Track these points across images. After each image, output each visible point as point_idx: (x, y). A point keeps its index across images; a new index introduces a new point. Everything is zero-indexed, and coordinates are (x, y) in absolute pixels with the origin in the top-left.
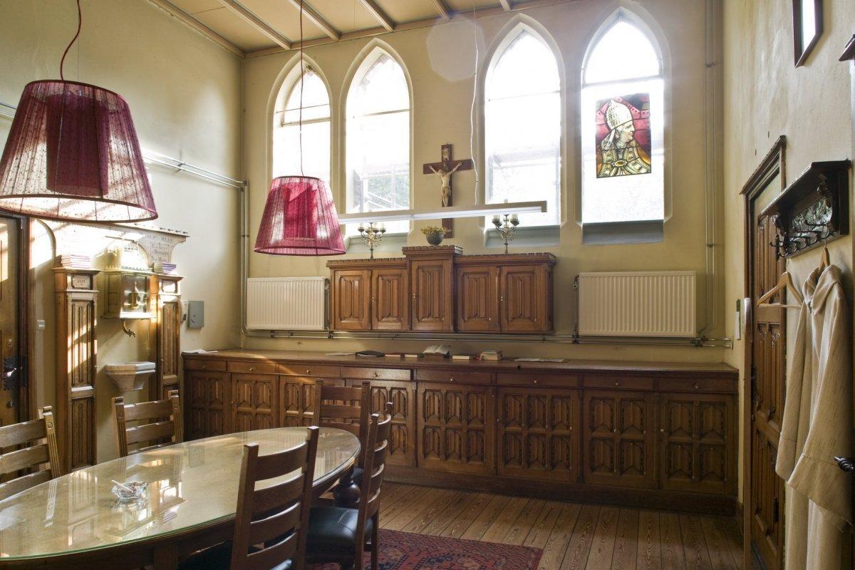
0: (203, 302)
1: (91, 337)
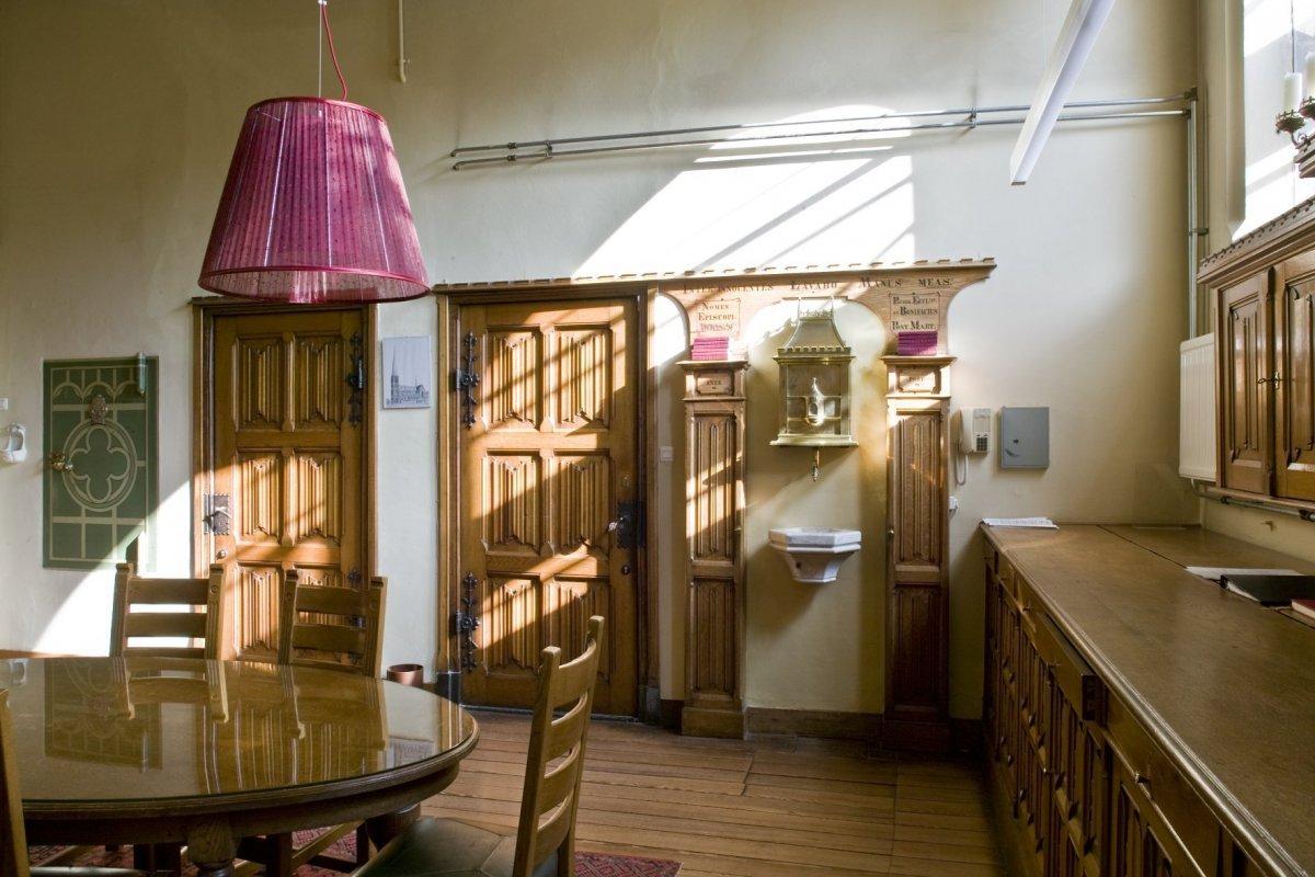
0: (1046, 410)
1: (730, 477)
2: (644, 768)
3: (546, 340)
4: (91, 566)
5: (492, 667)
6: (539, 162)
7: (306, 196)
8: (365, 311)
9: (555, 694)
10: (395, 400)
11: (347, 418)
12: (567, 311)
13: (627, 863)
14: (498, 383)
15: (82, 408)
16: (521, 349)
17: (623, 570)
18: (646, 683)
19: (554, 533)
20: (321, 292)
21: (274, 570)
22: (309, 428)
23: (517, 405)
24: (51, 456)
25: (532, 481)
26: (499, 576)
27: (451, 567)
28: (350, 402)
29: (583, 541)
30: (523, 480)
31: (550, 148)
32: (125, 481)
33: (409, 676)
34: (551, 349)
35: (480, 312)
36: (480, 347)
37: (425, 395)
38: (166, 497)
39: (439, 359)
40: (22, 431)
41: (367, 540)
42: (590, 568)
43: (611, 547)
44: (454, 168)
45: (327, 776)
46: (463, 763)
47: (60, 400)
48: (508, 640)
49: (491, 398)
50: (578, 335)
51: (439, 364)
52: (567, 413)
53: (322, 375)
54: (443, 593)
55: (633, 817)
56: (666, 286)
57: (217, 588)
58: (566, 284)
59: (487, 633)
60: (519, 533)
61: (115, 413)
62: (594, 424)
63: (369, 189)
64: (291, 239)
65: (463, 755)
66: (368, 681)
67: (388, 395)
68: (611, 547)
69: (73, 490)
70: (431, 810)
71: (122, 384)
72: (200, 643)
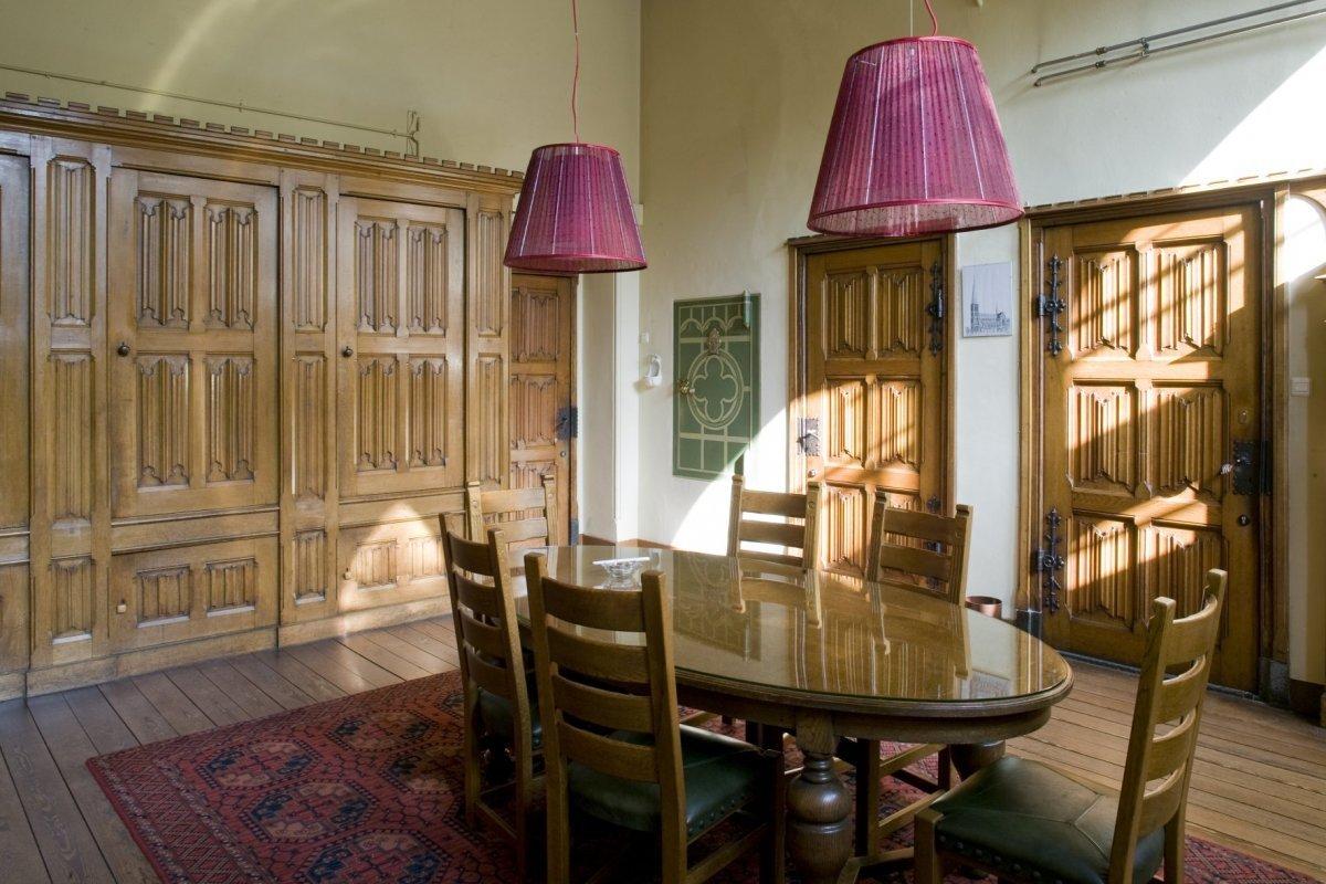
2: (1268, 756)
3: (1142, 260)
4: (712, 477)
5: (1076, 611)
6: (1135, 62)
7: (902, 134)
8: (944, 241)
9: (1168, 652)
10: (974, 328)
11: (927, 347)
12: (1171, 225)
13: (1248, 864)
14: (1086, 307)
15: (701, 340)
16: (1114, 275)
17: (1240, 520)
18: (1270, 655)
19: (1153, 473)
20: (913, 224)
21: (858, 491)
22: (891, 356)
23: (1108, 331)
24: (679, 382)
25: (1126, 415)
26: (1088, 515)
27: (1033, 501)
28: (931, 331)
29: (1188, 483)
30: (1115, 412)
31: (1146, 46)
32: (735, 402)
33: (990, 609)
34: (1148, 269)
35: (1065, 233)
36: (1066, 269)
37: (1005, 323)
38: (767, 422)
39: (1021, 285)
40: (659, 360)
41: (946, 468)
42: (1199, 515)
43: (1223, 492)
44: (1036, 85)
45: (903, 693)
46: (1055, 711)
47: (686, 334)
48: (1096, 585)
49: (1078, 325)
50: (1182, 252)
51: (1020, 290)
52: (1168, 339)
53: (903, 306)
54: (1024, 527)
55: (1253, 810)
56: (1298, 186)
57: (814, 503)
58: (1169, 194)
59: (1076, 572)
60: (1111, 470)
61: (727, 345)
62: (1201, 353)
63: (962, 119)
64: (890, 176)
65: (1056, 699)
66: (952, 606)
67: (967, 324)
68: (1223, 492)
69: (695, 411)
70: (1016, 750)
71: (734, 318)
72: (796, 552)
